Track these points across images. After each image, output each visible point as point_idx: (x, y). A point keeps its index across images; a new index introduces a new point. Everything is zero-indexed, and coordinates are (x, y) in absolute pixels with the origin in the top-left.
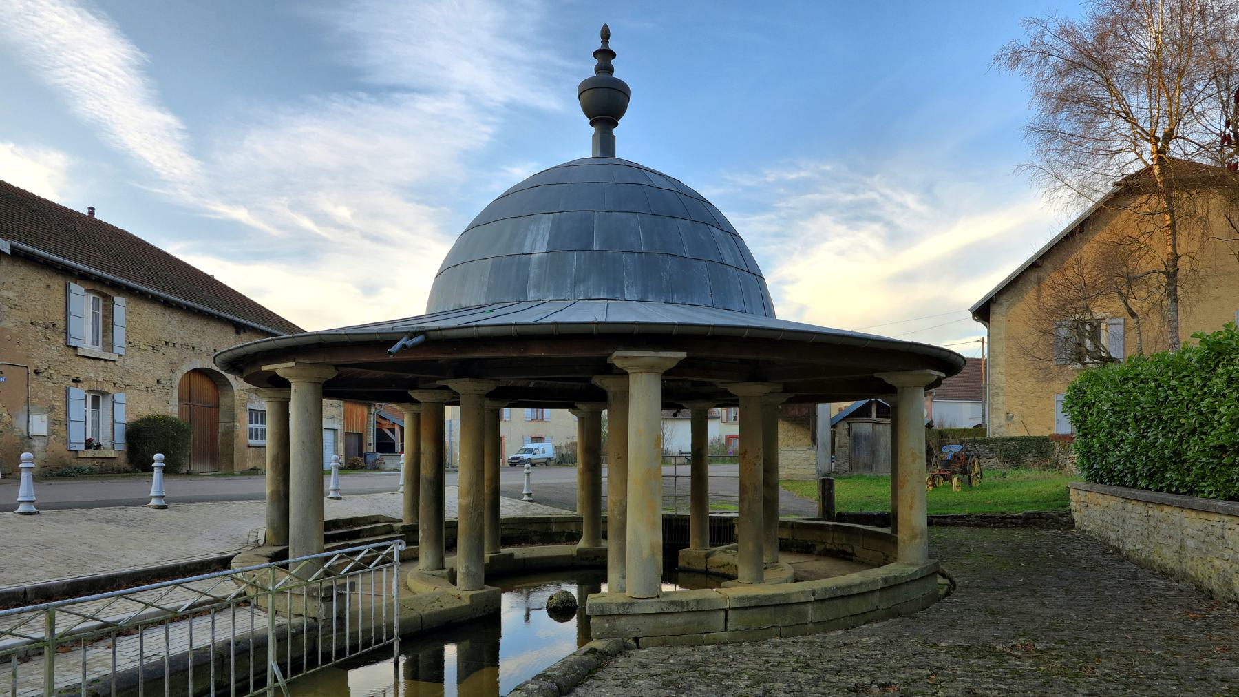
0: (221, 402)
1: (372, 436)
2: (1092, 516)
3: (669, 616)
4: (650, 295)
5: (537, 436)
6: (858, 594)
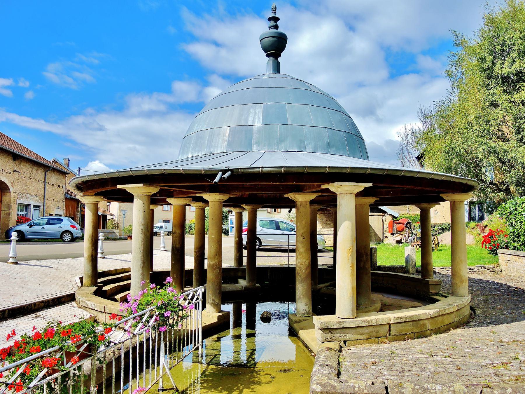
0: (3, 199)
1: (79, 219)
2: (515, 268)
3: (362, 329)
4: (319, 149)
5: (166, 219)
6: (448, 314)
